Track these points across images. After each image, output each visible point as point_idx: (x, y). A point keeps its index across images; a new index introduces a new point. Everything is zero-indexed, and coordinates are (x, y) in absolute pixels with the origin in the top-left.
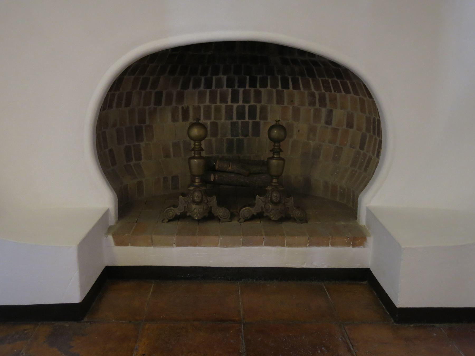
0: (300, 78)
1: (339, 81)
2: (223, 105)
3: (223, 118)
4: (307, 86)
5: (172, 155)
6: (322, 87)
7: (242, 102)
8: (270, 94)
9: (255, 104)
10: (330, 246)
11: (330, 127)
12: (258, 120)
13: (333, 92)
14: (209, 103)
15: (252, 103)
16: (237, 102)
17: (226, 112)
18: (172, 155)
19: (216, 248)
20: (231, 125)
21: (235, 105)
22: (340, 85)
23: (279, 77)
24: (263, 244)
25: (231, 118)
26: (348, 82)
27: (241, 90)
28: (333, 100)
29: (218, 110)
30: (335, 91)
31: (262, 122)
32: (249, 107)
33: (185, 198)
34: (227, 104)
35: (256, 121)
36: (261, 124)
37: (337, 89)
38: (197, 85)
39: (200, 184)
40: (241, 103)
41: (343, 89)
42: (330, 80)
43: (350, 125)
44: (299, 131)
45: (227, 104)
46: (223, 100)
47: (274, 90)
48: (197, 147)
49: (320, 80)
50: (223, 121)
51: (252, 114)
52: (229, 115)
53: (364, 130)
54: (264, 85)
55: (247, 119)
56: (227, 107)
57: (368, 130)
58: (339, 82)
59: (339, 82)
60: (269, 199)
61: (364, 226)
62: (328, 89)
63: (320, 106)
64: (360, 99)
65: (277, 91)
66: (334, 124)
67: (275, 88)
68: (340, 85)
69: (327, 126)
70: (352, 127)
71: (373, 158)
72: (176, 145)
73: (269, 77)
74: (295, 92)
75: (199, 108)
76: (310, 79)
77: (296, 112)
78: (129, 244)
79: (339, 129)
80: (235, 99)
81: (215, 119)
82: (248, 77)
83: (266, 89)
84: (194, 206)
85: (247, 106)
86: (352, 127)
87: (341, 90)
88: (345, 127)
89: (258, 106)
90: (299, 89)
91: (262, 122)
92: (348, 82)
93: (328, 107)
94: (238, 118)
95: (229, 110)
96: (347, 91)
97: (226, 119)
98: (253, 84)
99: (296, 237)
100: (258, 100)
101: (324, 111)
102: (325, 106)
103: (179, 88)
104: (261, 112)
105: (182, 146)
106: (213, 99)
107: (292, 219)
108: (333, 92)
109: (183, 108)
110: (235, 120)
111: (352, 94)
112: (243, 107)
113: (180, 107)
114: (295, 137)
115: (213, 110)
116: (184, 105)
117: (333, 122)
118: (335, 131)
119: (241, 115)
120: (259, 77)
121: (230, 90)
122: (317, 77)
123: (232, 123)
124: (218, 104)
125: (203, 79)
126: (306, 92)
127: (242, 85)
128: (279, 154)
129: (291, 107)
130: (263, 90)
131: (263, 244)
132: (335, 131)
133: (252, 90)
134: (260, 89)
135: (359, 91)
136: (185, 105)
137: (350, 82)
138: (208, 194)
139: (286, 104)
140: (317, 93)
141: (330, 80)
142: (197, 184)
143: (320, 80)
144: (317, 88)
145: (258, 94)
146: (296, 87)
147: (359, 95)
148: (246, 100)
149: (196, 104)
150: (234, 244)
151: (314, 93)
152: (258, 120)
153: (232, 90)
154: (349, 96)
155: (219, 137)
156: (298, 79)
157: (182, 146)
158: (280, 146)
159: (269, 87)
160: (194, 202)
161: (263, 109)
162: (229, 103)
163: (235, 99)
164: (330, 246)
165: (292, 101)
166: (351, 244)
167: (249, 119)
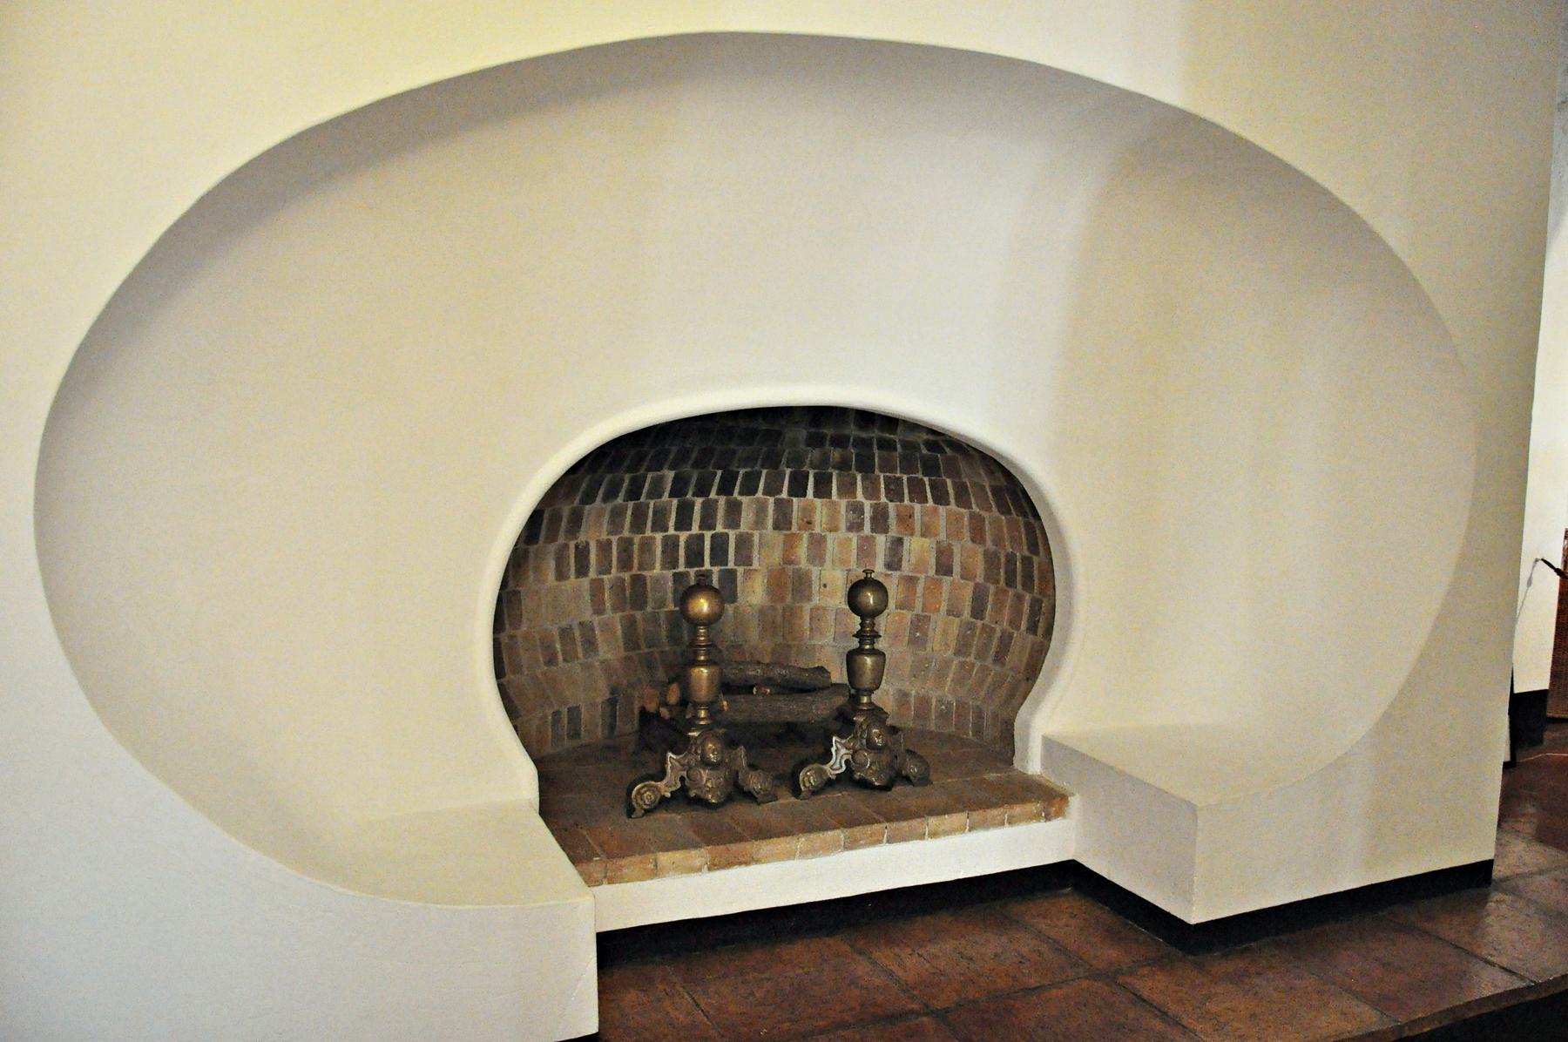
0: (835, 474)
1: (926, 479)
2: (659, 536)
3: (658, 565)
4: (847, 489)
5: (560, 658)
6: (883, 490)
7: (697, 528)
8: (761, 510)
9: (726, 531)
10: (1006, 824)
11: (897, 574)
12: (731, 565)
13: (907, 502)
14: (630, 532)
15: (719, 529)
16: (712, 527)
17: (663, 552)
18: (560, 658)
19: (791, 862)
20: (675, 581)
21: (683, 536)
22: (928, 488)
23: (788, 471)
24: (885, 840)
25: (674, 564)
26: (949, 482)
27: (699, 501)
28: (906, 519)
29: (647, 546)
30: (911, 500)
31: (740, 570)
32: (713, 537)
33: (681, 756)
34: (666, 534)
35: (728, 567)
36: (738, 574)
37: (918, 494)
38: (611, 495)
39: (709, 722)
40: (695, 529)
41: (933, 495)
42: (905, 477)
43: (944, 568)
44: (825, 586)
45: (666, 534)
46: (660, 525)
47: (771, 500)
48: (703, 639)
49: (882, 477)
50: (657, 571)
51: (719, 553)
52: (670, 561)
53: (980, 579)
54: (749, 489)
55: (707, 566)
56: (665, 539)
57: (991, 576)
58: (927, 483)
59: (927, 483)
60: (864, 741)
61: (1040, 776)
62: (894, 493)
63: (873, 530)
64: (972, 517)
65: (778, 503)
66: (906, 568)
67: (774, 496)
68: (928, 488)
69: (889, 572)
70: (949, 572)
71: (1015, 635)
72: (565, 633)
73: (764, 472)
74: (818, 502)
75: (609, 543)
76: (859, 477)
77: (817, 543)
78: (605, 881)
79: (919, 579)
80: (683, 523)
81: (639, 569)
82: (719, 473)
83: (752, 497)
84: (705, 774)
85: (708, 535)
86: (949, 572)
87: (926, 496)
88: (932, 572)
89: (732, 534)
90: (829, 495)
91: (740, 570)
92: (949, 482)
93: (894, 531)
94: (689, 564)
95: (671, 545)
96: (941, 498)
97: (663, 567)
98: (726, 489)
99: (946, 816)
100: (733, 522)
101: (881, 541)
102: (885, 530)
103: (577, 501)
104: (737, 547)
105: (577, 634)
106: (638, 526)
107: (907, 780)
108: (907, 502)
109: (577, 547)
110: (681, 568)
111: (953, 506)
112: (701, 537)
113: (572, 544)
114: (816, 600)
115: (636, 547)
116: (579, 541)
117: (904, 564)
118: (911, 581)
119: (695, 557)
120: (742, 472)
121: (675, 502)
122: (877, 472)
123: (675, 575)
124: (648, 533)
125: (627, 478)
126: (843, 503)
127: (702, 491)
128: (872, 643)
129: (805, 535)
130: (745, 500)
131: (885, 840)
132: (911, 581)
133: (722, 500)
134: (739, 498)
135: (973, 500)
136: (582, 538)
137: (954, 484)
138: (730, 743)
139: (794, 528)
140: (868, 506)
141: (905, 477)
142: (702, 723)
143: (882, 477)
144: (871, 493)
145: (734, 510)
146: (822, 490)
147: (971, 507)
148: (707, 523)
149: (604, 537)
150: (828, 849)
151: (862, 505)
152: (731, 565)
153: (679, 501)
154: (942, 509)
155: (649, 609)
156: (831, 475)
157: (577, 634)
158: (874, 624)
159: (760, 494)
160: (706, 763)
161: (744, 542)
162: (671, 531)
163: (683, 523)
164: (1006, 824)
165: (809, 523)
166: (1043, 815)
167: (712, 564)
